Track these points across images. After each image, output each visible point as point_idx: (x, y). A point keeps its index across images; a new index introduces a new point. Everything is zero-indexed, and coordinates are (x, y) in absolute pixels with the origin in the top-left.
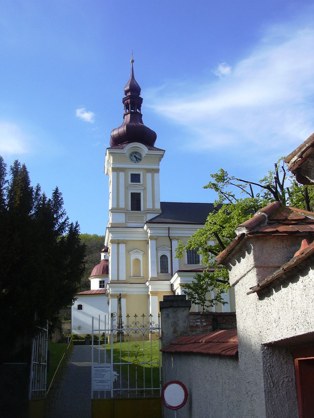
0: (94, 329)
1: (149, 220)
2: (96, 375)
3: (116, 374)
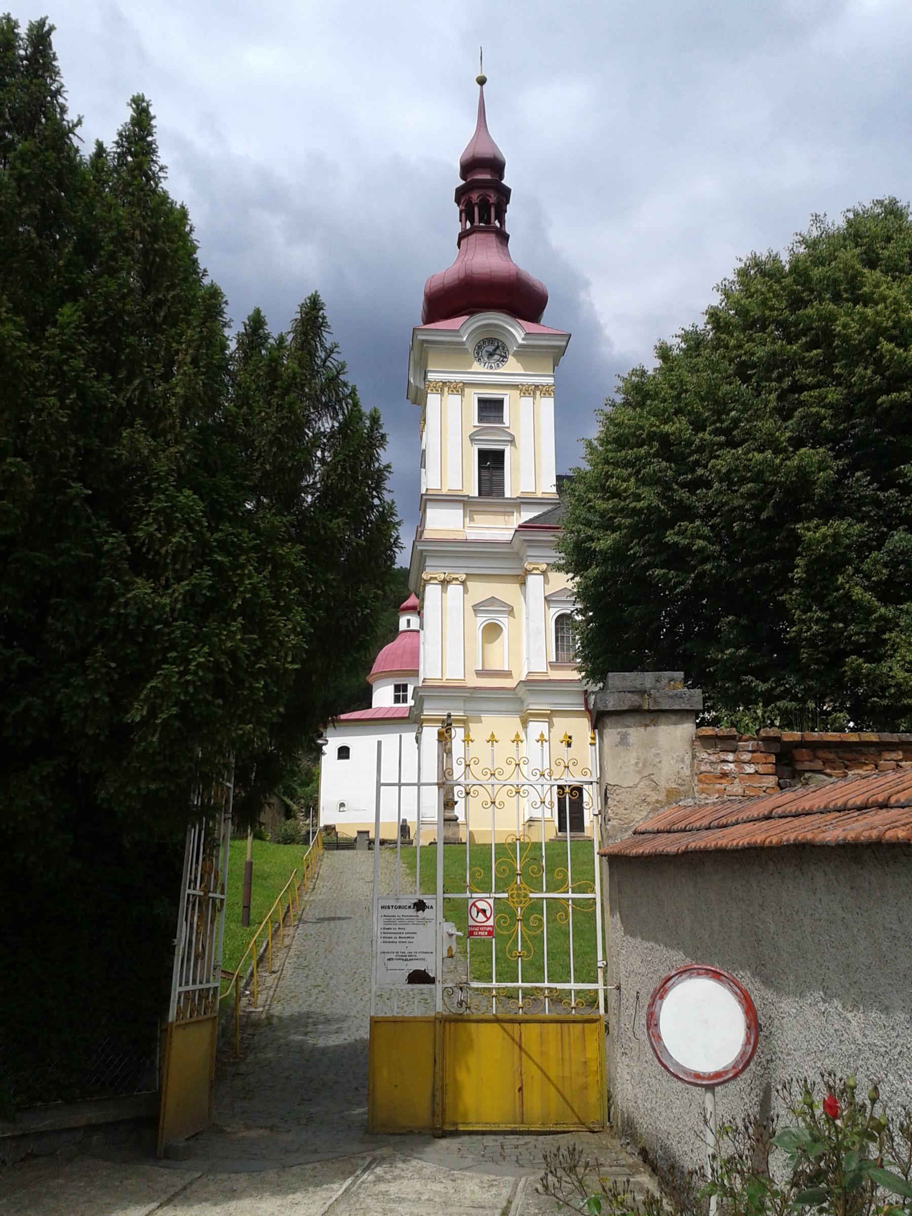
0: (382, 781)
1: (526, 522)
2: (387, 935)
3: (453, 931)
